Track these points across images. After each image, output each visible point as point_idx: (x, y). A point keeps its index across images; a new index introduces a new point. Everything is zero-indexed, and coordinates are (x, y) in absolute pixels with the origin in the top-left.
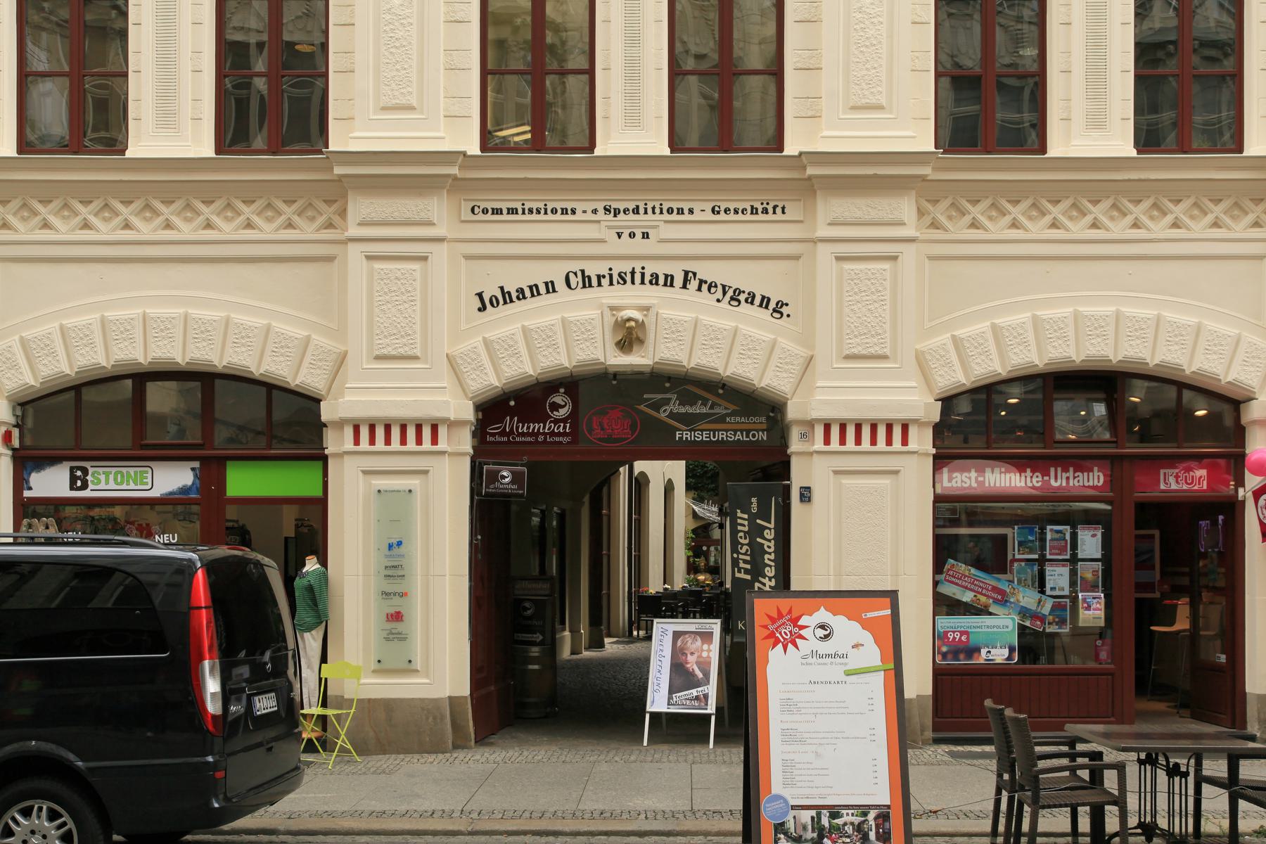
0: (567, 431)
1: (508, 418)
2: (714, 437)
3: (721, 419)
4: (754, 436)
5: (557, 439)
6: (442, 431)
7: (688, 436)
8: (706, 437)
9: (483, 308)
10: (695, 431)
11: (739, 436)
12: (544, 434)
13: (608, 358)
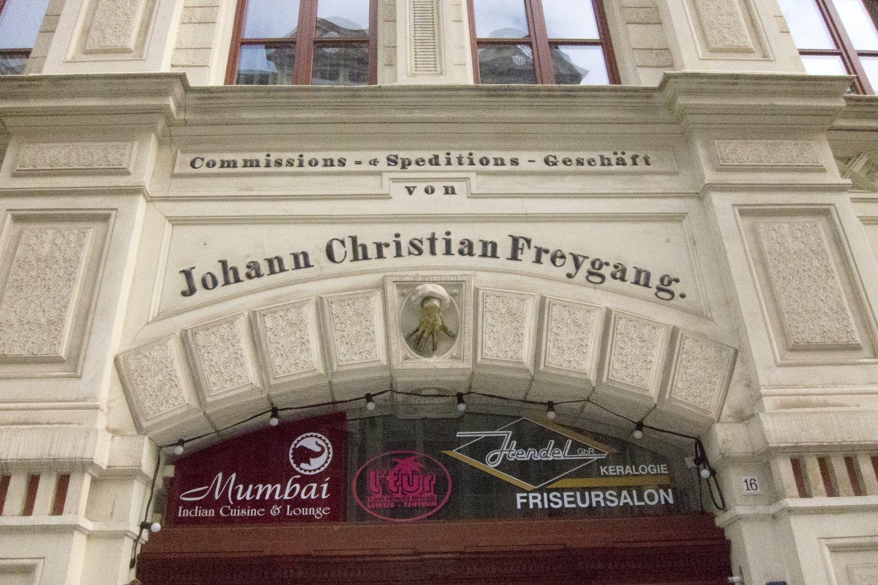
0: (324, 496)
1: (220, 475)
2: (583, 501)
3: (588, 470)
5: (304, 511)
7: (538, 501)
8: (569, 502)
10: (549, 492)
11: (625, 498)
12: (282, 503)
13: (394, 362)
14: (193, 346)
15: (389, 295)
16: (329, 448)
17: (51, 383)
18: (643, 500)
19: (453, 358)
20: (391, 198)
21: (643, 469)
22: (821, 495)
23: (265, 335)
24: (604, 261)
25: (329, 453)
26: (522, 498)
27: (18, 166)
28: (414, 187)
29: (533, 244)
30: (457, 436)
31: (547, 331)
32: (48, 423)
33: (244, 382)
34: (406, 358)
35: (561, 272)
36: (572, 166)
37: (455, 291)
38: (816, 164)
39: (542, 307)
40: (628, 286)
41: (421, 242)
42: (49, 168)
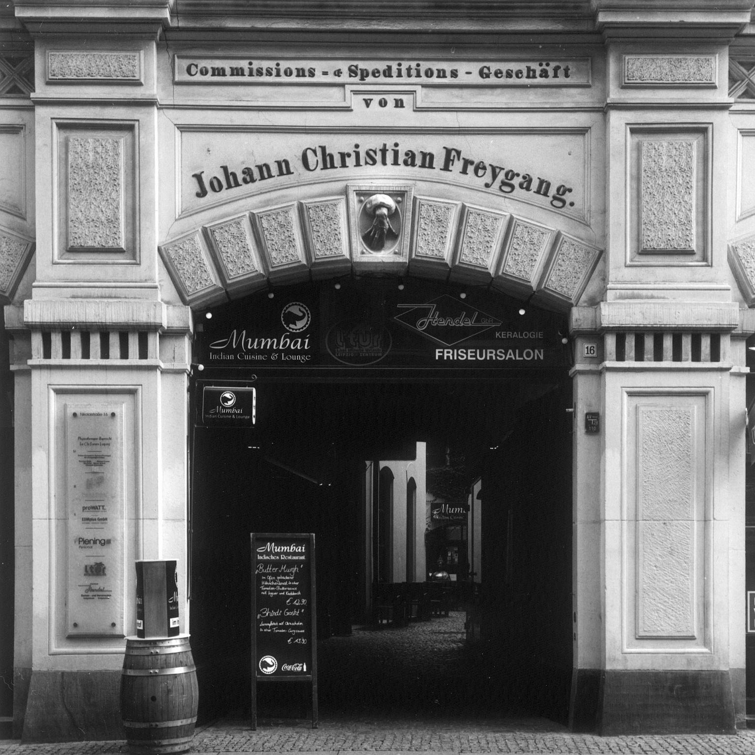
2: (481, 356)
4: (528, 355)
5: (293, 358)
6: (154, 341)
7: (450, 355)
8: (471, 356)
9: (202, 193)
11: (510, 355)
12: (278, 351)
14: (213, 242)
15: (351, 203)
16: (308, 314)
17: (120, 268)
18: (522, 356)
19: (395, 253)
20: (352, 110)
21: (526, 335)
22: (631, 359)
23: (263, 233)
24: (516, 172)
25: (308, 317)
26: (439, 352)
27: (50, 75)
28: (371, 100)
29: (462, 156)
30: (368, 463)
31: (464, 234)
32: (126, 298)
33: (251, 270)
34: (363, 253)
35: (480, 182)
36: (501, 79)
37: (399, 199)
38: (709, 82)
39: (463, 213)
40: (531, 195)
41: (375, 152)
42: (75, 77)
